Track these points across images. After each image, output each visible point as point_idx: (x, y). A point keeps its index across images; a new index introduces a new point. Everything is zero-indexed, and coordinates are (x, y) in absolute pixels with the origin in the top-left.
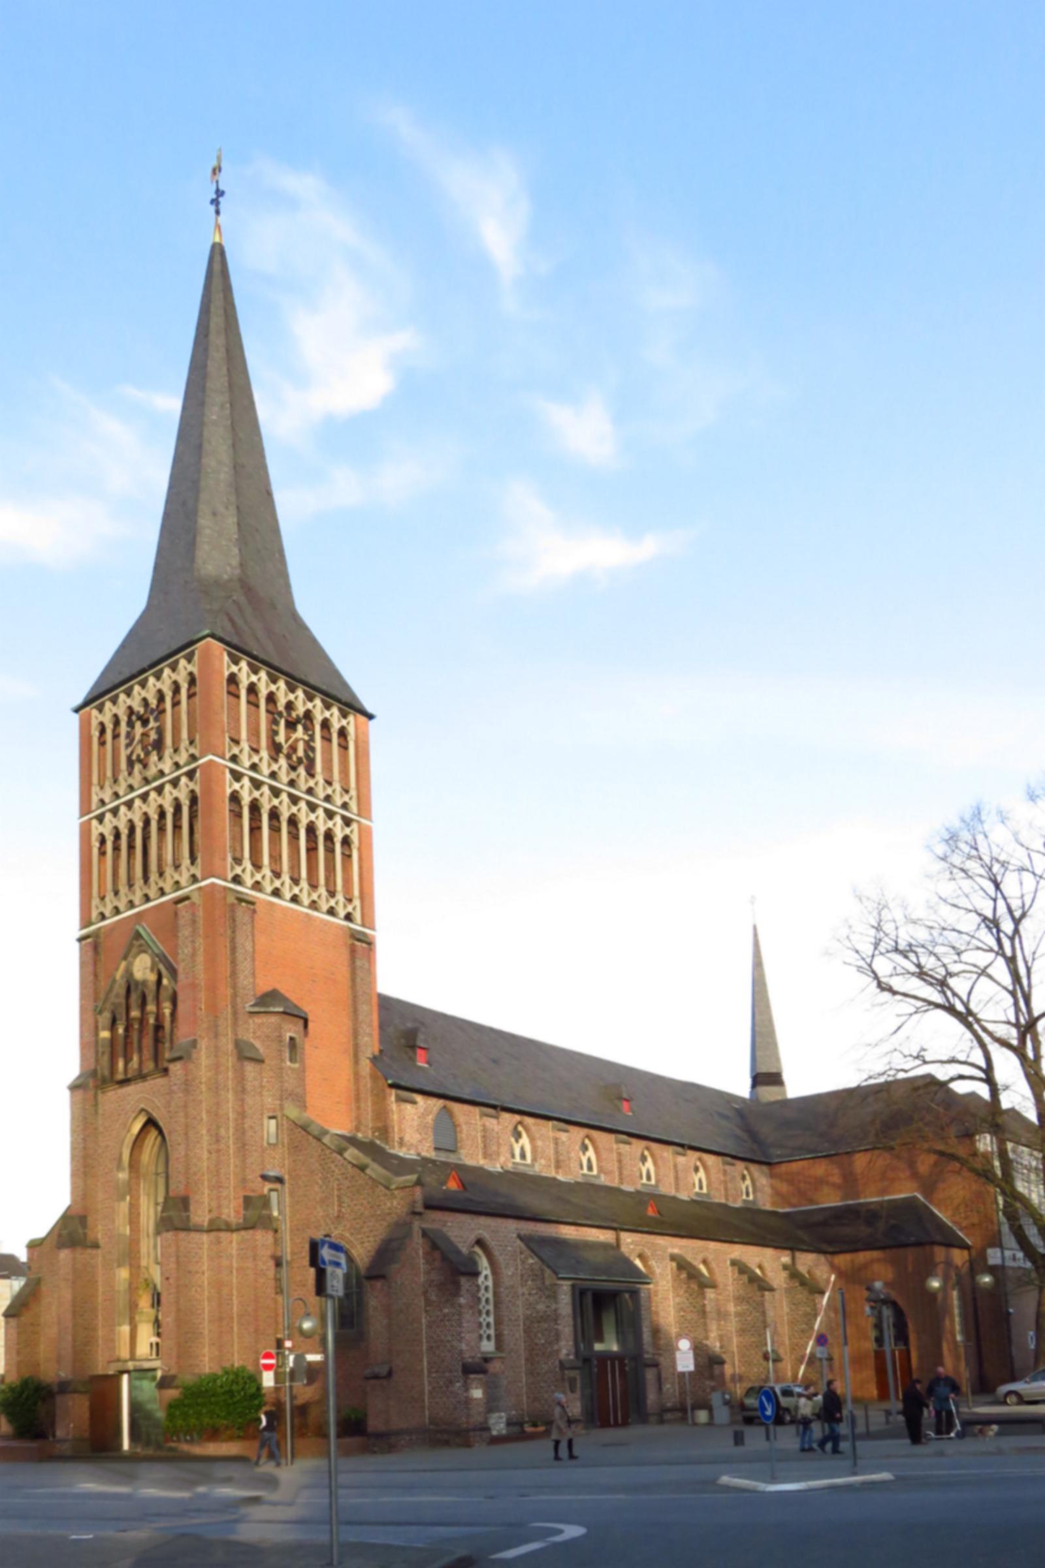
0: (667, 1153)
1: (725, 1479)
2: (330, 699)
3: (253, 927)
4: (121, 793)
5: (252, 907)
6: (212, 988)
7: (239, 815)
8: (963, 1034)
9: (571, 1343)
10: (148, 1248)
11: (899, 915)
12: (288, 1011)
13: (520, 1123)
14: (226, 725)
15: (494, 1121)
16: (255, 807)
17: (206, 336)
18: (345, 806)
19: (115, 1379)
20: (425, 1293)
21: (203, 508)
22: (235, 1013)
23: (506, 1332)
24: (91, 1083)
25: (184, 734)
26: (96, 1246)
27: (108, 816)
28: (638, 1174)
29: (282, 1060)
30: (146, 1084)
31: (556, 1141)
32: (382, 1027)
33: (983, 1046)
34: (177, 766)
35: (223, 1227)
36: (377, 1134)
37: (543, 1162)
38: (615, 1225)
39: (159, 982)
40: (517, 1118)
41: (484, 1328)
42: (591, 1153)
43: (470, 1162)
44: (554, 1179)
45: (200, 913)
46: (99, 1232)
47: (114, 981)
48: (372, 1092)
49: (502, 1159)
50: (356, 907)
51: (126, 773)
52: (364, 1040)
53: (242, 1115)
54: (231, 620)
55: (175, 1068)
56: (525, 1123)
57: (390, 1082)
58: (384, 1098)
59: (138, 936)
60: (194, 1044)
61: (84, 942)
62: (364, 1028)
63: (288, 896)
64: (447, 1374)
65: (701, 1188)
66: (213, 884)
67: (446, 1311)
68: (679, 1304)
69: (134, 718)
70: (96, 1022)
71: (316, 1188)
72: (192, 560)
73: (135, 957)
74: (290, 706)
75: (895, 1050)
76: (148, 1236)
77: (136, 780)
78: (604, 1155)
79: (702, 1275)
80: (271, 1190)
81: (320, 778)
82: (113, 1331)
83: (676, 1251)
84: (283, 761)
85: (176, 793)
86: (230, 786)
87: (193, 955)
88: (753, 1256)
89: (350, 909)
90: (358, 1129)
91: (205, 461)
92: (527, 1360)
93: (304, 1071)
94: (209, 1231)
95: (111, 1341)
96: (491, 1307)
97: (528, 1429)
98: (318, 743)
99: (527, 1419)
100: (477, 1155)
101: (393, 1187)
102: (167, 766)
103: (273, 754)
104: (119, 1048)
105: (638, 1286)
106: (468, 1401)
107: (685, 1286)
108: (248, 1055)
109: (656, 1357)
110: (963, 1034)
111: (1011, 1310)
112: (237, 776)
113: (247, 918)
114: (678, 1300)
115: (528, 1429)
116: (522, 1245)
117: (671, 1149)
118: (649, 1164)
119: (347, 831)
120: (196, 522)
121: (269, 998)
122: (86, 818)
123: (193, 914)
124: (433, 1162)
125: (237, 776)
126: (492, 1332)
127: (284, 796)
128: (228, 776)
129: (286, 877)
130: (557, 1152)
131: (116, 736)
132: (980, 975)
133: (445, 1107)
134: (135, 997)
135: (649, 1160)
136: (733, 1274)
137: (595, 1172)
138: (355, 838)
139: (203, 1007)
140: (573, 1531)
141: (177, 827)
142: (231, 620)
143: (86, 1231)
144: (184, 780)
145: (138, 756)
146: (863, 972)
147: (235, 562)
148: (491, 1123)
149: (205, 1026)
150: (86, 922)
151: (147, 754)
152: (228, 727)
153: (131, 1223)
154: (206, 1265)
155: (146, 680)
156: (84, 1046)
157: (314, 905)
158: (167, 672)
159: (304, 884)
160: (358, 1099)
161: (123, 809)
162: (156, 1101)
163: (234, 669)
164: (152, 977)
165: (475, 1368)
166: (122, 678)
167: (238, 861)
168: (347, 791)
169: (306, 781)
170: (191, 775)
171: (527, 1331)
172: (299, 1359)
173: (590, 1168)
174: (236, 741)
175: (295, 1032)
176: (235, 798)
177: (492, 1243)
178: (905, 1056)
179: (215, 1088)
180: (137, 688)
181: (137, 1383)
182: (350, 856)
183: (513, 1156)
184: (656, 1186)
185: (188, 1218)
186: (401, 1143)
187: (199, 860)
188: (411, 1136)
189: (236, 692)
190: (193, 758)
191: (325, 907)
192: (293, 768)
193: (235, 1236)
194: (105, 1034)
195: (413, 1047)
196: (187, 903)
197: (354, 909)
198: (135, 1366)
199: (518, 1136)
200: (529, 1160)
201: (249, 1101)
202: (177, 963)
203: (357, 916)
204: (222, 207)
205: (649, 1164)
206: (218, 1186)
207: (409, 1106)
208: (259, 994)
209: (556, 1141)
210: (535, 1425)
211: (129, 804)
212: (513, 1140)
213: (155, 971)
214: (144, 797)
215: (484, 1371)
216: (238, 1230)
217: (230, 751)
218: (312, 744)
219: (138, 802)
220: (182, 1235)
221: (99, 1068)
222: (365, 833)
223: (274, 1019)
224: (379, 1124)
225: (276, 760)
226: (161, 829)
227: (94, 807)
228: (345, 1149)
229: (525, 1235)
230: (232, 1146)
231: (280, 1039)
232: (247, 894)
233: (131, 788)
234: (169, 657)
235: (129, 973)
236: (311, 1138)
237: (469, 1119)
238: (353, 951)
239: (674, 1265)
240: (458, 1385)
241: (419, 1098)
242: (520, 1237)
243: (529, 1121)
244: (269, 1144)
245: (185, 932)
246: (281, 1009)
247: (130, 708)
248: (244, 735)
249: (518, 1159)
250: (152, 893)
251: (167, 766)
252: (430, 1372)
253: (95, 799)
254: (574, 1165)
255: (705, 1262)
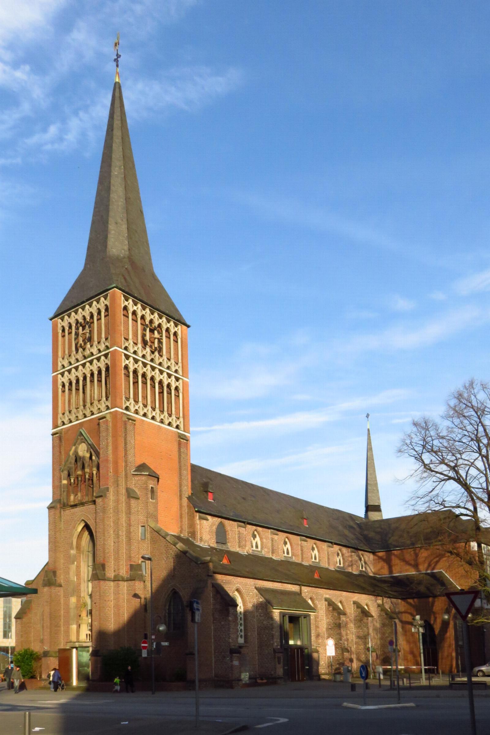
0: (324, 546)
1: (345, 704)
2: (170, 318)
3: (134, 432)
4: (72, 362)
5: (134, 422)
6: (116, 463)
7: (128, 376)
8: (464, 493)
9: (279, 640)
10: (84, 588)
11: (433, 433)
12: (151, 474)
13: (256, 530)
14: (123, 331)
15: (244, 529)
16: (135, 372)
17: (112, 130)
18: (176, 371)
19: (70, 650)
20: (213, 614)
21: (111, 221)
22: (126, 475)
23: (249, 634)
24: (58, 506)
25: (103, 336)
26: (60, 586)
27: (66, 373)
28: (310, 556)
29: (148, 498)
30: (84, 507)
31: (272, 540)
32: (192, 481)
33: (473, 500)
34: (100, 351)
35: (121, 579)
36: (190, 535)
37: (266, 550)
38: (300, 583)
39: (91, 458)
40: (254, 527)
41: (239, 632)
42: (288, 545)
43: (232, 549)
44: (271, 558)
45: (110, 424)
46: (61, 579)
47: (69, 456)
48: (188, 514)
49: (247, 548)
50: (181, 422)
51: (75, 352)
52: (185, 488)
53: (129, 525)
54: (125, 279)
55: (99, 501)
56: (258, 530)
57: (196, 509)
58: (194, 517)
59: (81, 434)
60: (107, 489)
61: (54, 436)
62: (184, 482)
63: (150, 417)
64: (223, 654)
65: (340, 564)
66: (116, 411)
67: (223, 623)
68: (328, 622)
69: (79, 325)
70: (61, 476)
71: (163, 562)
72: (106, 246)
73: (79, 444)
74: (151, 321)
75: (431, 500)
76: (84, 582)
77: (80, 356)
78: (295, 547)
79: (340, 609)
80: (142, 562)
81: (165, 357)
82: (68, 628)
83: (327, 596)
84: (148, 349)
85: (99, 364)
86: (124, 362)
87: (107, 446)
88: (365, 600)
89: (178, 423)
90: (181, 532)
91: (111, 195)
92: (258, 647)
93: (157, 504)
94: (114, 581)
95: (67, 632)
96: (242, 622)
97: (259, 681)
98: (164, 340)
99: (258, 676)
100: (236, 546)
101: (199, 562)
102: (95, 350)
103: (143, 345)
104: (73, 488)
105: (310, 613)
106: (232, 666)
107: (331, 614)
108: (132, 495)
109: (317, 648)
110: (464, 493)
111: (485, 630)
112: (127, 357)
113: (132, 428)
114: (328, 620)
115: (259, 681)
116: (257, 592)
117: (326, 544)
118: (316, 551)
119: (177, 384)
120: (108, 227)
121: (142, 467)
122: (55, 373)
123: (107, 426)
124: (216, 549)
125: (127, 357)
126: (243, 634)
127: (149, 367)
128: (123, 357)
129: (149, 407)
130: (272, 545)
131: (70, 333)
132: (470, 466)
133: (221, 522)
134: (80, 464)
135: (316, 549)
136: (354, 609)
137: (290, 555)
138: (181, 388)
139: (111, 471)
140: (283, 720)
141: (100, 381)
142: (125, 279)
143: (56, 578)
144: (103, 358)
145: (81, 344)
146: (418, 460)
147: (126, 248)
148: (242, 530)
149: (112, 480)
150: (55, 426)
151: (85, 344)
152: (123, 332)
153: (77, 575)
154: (113, 597)
155: (85, 306)
156: (54, 487)
157: (162, 422)
158: (95, 303)
159: (157, 410)
160: (181, 517)
161: (73, 370)
162: (89, 516)
163: (126, 303)
164: (88, 455)
165: (236, 651)
166: (73, 305)
167: (128, 399)
168: (177, 364)
169: (159, 359)
170: (106, 356)
171: (259, 634)
172: (158, 645)
173: (288, 553)
174: (127, 340)
175: (153, 485)
176: (126, 367)
177: (243, 591)
178: (436, 504)
179: (117, 511)
180: (80, 310)
181: (81, 653)
182: (178, 396)
183: (252, 547)
184: (319, 562)
185: (105, 573)
186: (201, 540)
187: (110, 398)
188: (206, 537)
189: (127, 315)
190: (107, 348)
191: (167, 422)
192: (153, 352)
193: (126, 583)
194: (65, 482)
195: (207, 492)
196: (104, 419)
197: (180, 423)
198: (79, 645)
199: (254, 537)
200: (259, 549)
201: (133, 518)
202: (99, 449)
203: (182, 426)
204: (119, 63)
205: (316, 551)
206: (117, 559)
207: (205, 522)
208: (137, 465)
209: (272, 540)
210: (262, 679)
211: (76, 368)
212: (252, 538)
213: (89, 452)
214: (84, 365)
215: (239, 653)
216: (127, 581)
217: (124, 345)
218: (161, 340)
219: (80, 368)
220: (102, 582)
221: (62, 498)
222: (185, 384)
223: (144, 478)
224: (191, 530)
225: (145, 349)
226: (92, 381)
227: (59, 369)
228: (177, 543)
229: (258, 587)
230: (124, 540)
231: (146, 488)
232: (132, 416)
233: (77, 360)
234: (96, 296)
235: (76, 453)
236: (161, 537)
237: (231, 527)
238: (180, 444)
239: (327, 603)
240: (228, 658)
241: (209, 517)
242: (256, 588)
243: (259, 529)
244: (141, 539)
245: (103, 434)
246: (147, 474)
247: (77, 320)
248: (131, 336)
249: (254, 548)
250: (88, 413)
251: (95, 350)
252: (215, 652)
253: (60, 365)
254: (280, 552)
255: (341, 602)
